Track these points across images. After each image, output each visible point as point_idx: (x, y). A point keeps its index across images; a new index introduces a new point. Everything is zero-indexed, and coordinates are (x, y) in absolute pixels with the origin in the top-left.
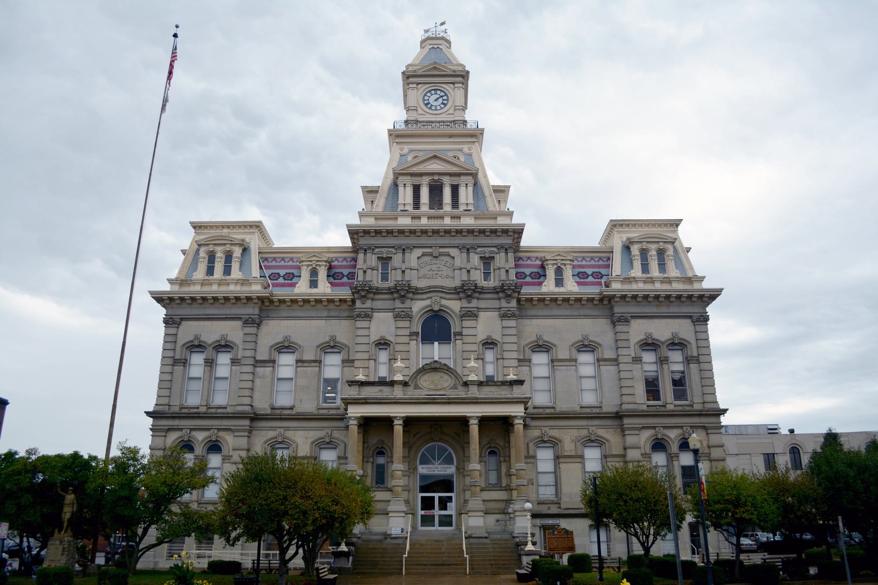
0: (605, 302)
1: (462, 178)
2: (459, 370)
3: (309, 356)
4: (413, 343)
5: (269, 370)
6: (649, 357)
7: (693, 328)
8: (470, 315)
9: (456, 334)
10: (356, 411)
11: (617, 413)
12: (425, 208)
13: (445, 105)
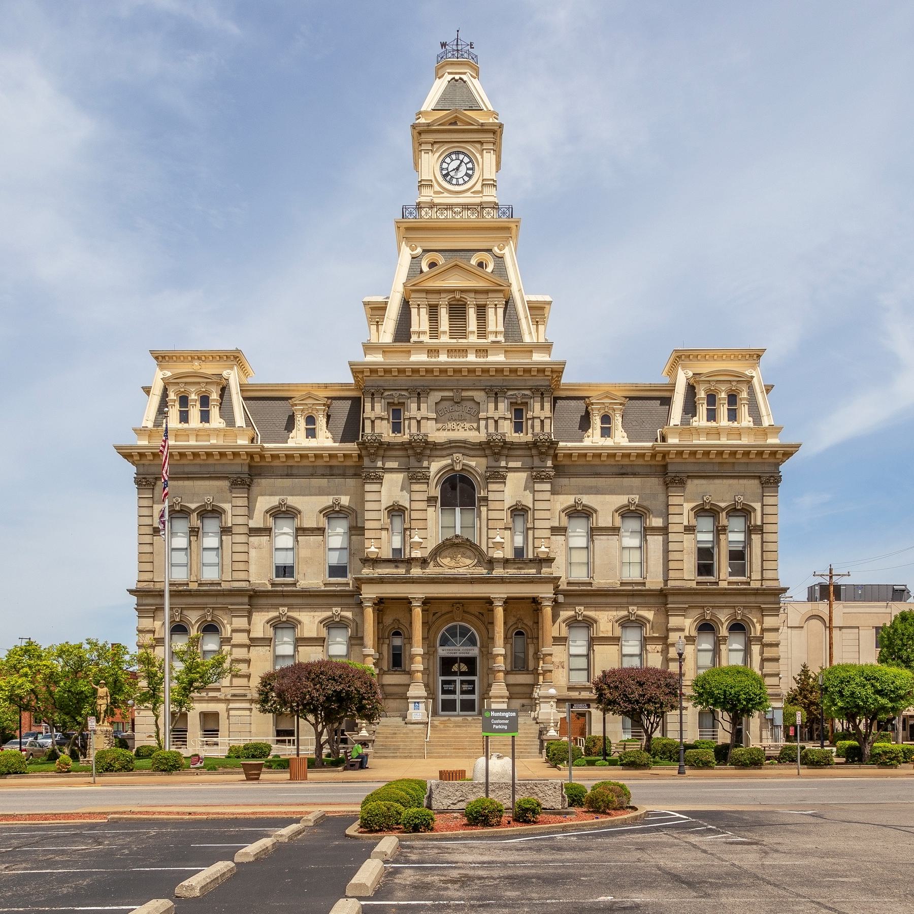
0: (659, 458)
1: (490, 295)
2: (484, 548)
3: (309, 521)
4: (431, 510)
5: (264, 539)
6: (706, 523)
7: (760, 491)
8: (496, 476)
10: (370, 593)
11: (661, 590)
13: (470, 176)
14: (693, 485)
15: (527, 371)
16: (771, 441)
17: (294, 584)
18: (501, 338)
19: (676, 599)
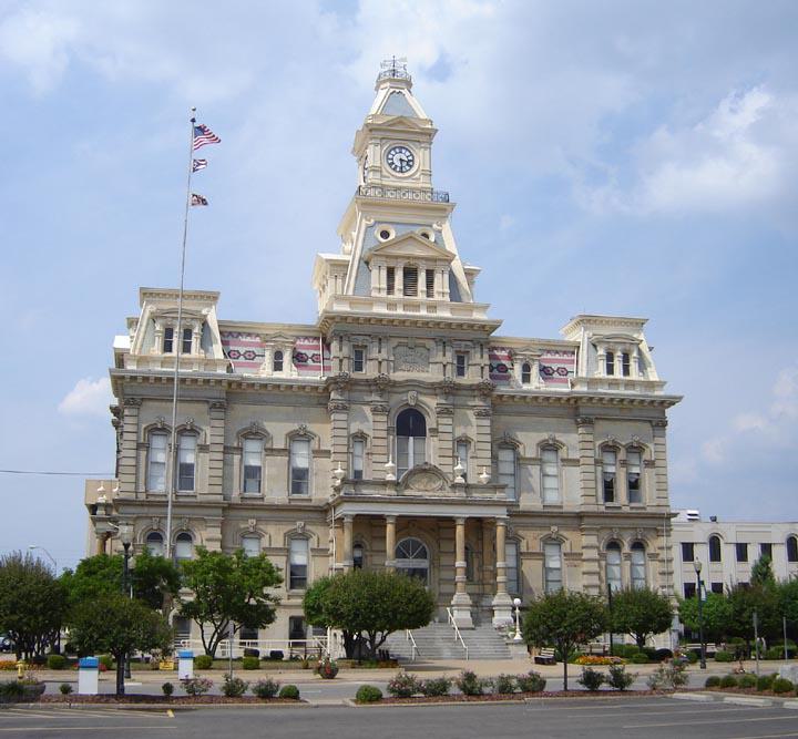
0: (572, 402)
3: (279, 444)
9: (432, 430)
10: (349, 510)
12: (398, 295)
14: (601, 426)
15: (471, 326)
16: (656, 393)
17: (262, 499)
18: (447, 298)
19: (591, 520)
